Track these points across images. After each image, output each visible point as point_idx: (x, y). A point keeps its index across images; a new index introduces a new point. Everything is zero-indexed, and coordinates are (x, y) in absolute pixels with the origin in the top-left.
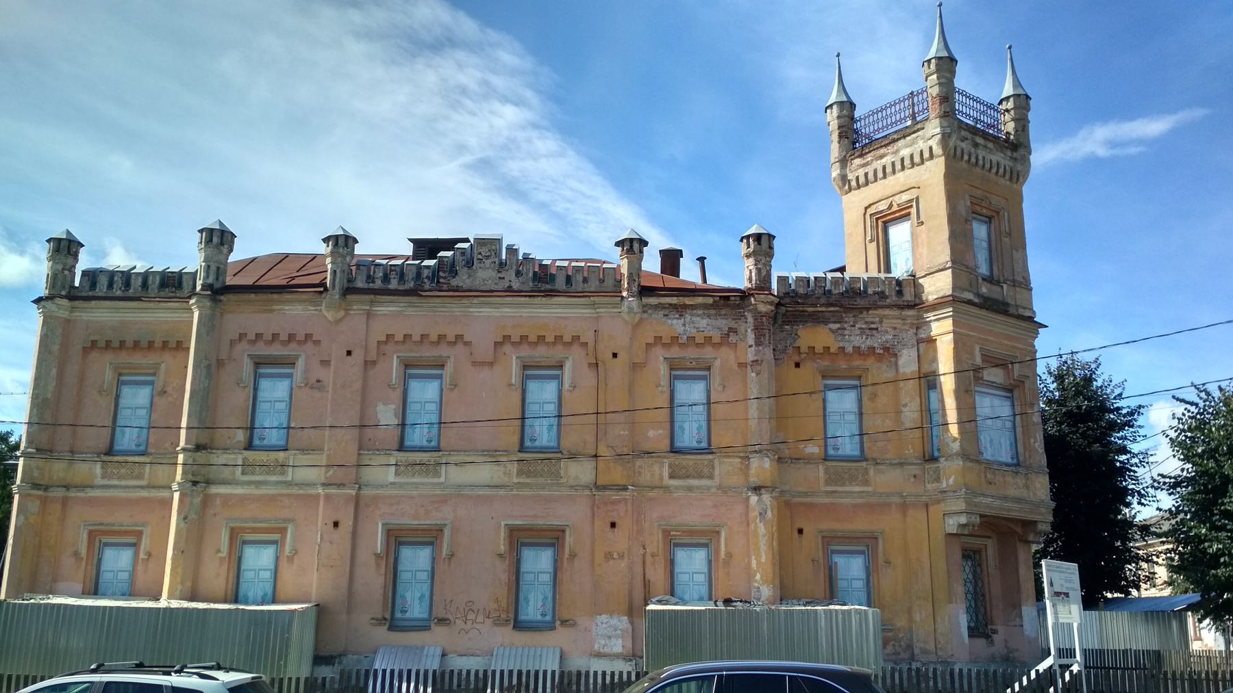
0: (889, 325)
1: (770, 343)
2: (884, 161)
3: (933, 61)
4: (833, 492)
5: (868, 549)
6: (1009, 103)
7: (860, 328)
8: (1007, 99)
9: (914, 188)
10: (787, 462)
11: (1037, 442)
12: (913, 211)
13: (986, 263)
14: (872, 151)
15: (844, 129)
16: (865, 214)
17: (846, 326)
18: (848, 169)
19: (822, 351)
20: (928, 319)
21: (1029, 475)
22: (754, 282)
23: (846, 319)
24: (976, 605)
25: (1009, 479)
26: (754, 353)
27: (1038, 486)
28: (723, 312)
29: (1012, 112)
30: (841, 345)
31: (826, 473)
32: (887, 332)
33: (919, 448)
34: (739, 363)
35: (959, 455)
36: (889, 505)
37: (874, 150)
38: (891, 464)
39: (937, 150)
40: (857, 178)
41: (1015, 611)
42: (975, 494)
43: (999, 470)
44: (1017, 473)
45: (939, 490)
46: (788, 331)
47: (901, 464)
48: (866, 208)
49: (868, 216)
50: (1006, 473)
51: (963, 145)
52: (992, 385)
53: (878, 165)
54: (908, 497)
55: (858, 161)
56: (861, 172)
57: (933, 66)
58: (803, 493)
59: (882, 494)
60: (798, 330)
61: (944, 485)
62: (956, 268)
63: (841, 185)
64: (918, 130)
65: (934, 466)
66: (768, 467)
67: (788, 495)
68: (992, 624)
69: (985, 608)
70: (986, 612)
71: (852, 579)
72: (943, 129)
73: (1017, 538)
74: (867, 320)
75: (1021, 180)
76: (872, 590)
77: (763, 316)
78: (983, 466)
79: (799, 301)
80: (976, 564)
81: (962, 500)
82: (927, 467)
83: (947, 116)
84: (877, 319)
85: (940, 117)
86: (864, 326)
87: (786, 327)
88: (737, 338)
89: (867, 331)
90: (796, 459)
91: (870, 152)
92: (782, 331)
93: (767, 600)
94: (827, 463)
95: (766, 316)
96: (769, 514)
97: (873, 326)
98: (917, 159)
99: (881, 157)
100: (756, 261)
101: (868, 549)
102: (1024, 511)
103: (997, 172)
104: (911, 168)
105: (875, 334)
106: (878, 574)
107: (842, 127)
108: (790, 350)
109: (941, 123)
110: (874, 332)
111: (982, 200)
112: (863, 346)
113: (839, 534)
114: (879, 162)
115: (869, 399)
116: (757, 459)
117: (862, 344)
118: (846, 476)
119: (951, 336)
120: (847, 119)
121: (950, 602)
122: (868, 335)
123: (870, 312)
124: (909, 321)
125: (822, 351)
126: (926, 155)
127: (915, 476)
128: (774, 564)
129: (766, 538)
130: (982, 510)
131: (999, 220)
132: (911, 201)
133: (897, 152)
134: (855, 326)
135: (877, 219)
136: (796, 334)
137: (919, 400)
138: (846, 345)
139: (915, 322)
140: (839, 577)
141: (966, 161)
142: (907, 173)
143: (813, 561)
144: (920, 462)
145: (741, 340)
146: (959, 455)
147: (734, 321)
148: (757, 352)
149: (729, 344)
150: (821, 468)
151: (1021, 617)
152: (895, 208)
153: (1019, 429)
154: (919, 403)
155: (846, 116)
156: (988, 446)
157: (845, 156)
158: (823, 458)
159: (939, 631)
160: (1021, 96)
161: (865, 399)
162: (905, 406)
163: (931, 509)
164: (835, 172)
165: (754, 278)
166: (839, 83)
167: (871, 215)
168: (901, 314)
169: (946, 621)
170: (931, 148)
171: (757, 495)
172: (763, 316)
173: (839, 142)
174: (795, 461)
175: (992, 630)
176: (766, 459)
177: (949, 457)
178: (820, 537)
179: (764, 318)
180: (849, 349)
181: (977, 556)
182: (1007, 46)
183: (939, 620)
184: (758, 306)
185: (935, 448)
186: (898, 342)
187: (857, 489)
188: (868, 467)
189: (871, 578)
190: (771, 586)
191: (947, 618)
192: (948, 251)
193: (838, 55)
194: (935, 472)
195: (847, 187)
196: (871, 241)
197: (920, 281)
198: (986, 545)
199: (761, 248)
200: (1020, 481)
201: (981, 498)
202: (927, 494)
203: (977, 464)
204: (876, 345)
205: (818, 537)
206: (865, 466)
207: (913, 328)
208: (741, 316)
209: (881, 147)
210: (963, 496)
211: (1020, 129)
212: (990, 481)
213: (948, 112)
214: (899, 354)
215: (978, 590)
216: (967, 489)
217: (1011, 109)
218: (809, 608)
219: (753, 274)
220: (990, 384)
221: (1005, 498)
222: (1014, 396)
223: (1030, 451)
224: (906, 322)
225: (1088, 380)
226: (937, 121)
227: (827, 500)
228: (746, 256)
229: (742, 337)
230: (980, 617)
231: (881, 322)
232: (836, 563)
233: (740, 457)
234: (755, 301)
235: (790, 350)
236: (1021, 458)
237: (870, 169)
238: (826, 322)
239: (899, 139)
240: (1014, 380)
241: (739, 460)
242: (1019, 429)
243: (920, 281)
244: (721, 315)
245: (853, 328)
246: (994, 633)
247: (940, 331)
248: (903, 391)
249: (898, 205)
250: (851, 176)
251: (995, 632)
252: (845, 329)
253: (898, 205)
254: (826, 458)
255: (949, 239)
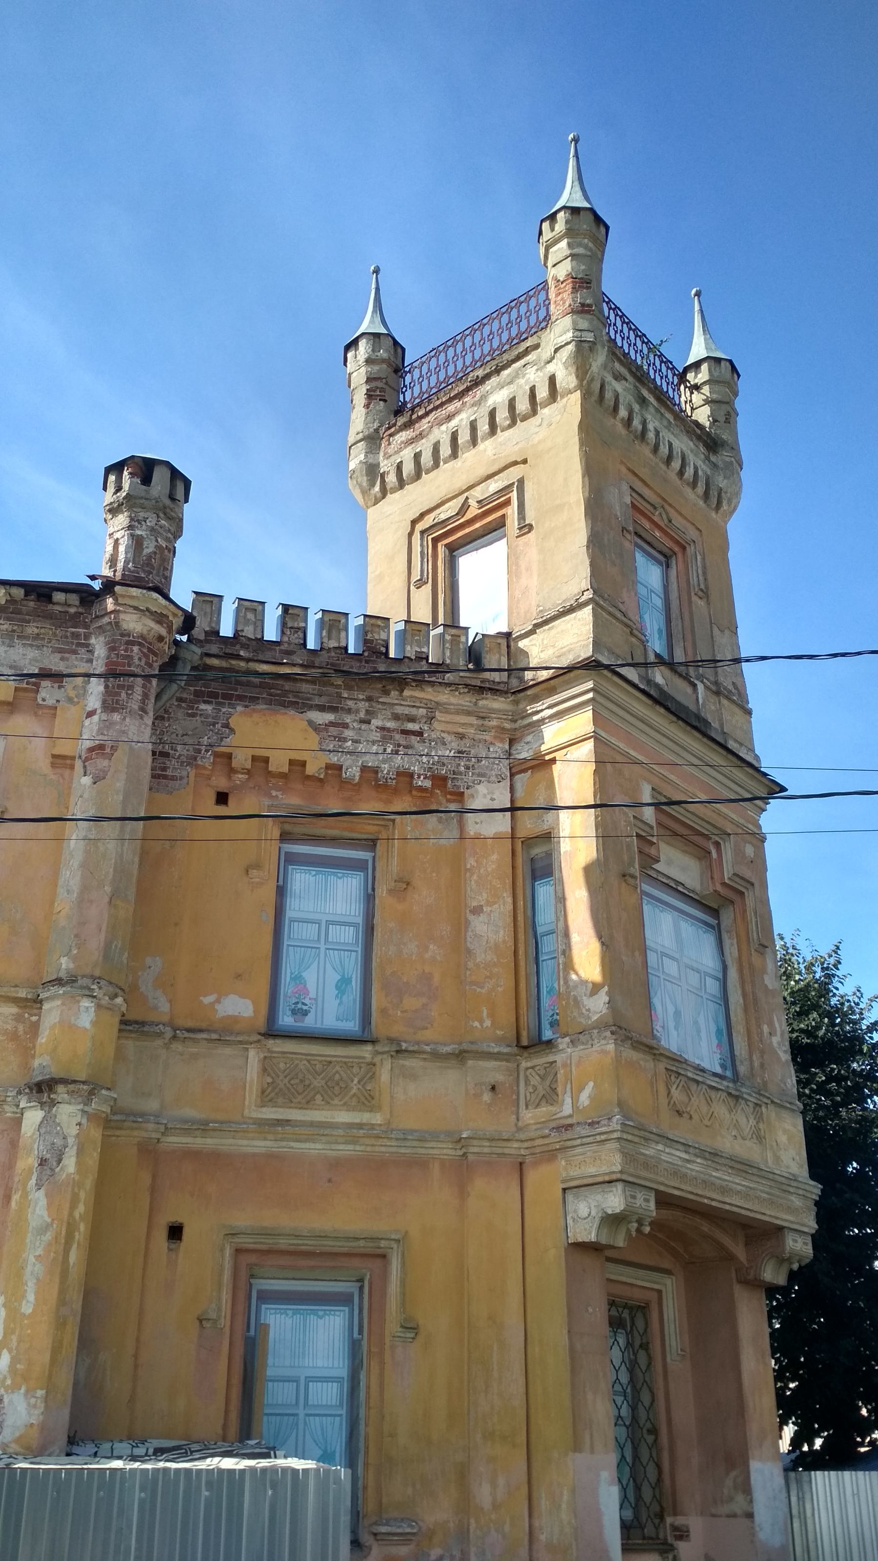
0: (450, 727)
1: (143, 710)
2: (454, 423)
3: (561, 216)
4: (279, 1122)
5: (361, 1288)
6: (700, 376)
7: (383, 729)
8: (697, 365)
9: (515, 463)
10: (160, 1035)
11: (775, 1035)
12: (512, 512)
13: (660, 638)
14: (431, 411)
15: (379, 384)
16: (410, 535)
17: (348, 719)
18: (382, 454)
19: (285, 769)
20: (535, 718)
21: (764, 1109)
22: (120, 565)
23: (350, 703)
24: (636, 1456)
25: (721, 1110)
26: (96, 728)
27: (783, 1139)
28: (31, 629)
29: (706, 390)
30: (334, 759)
31: (265, 1070)
32: (444, 744)
33: (507, 1017)
34: (54, 756)
35: (607, 1026)
36: (421, 1164)
37: (436, 408)
38: (436, 1056)
39: (566, 378)
40: (399, 467)
41: (733, 1474)
42: (647, 1135)
43: (697, 1082)
44: (737, 1098)
45: (553, 1124)
46: (207, 717)
47: (461, 1056)
48: (414, 523)
49: (417, 536)
50: (713, 1094)
51: (618, 387)
52: (674, 888)
53: (442, 434)
54: (475, 1142)
55: (404, 436)
56: (407, 455)
57: (560, 226)
58: (193, 1122)
59: (405, 1132)
60: (231, 714)
61: (567, 1109)
62: (602, 607)
63: (365, 484)
64: (527, 352)
65: (541, 1060)
66: (88, 1025)
67: (151, 1126)
68: (675, 1514)
69: (659, 1467)
70: (659, 1480)
71: (309, 1379)
72: (578, 334)
73: (734, 1275)
74: (399, 710)
75: (725, 506)
76: (362, 1412)
77: (133, 643)
78: (661, 1066)
79: (242, 653)
80: (637, 1343)
81: (614, 1145)
82: (524, 1064)
83: (588, 312)
84: (422, 712)
85: (573, 312)
86: (390, 724)
87: (203, 706)
88: (59, 694)
89: (398, 737)
90: (189, 1030)
91: (427, 414)
92: (193, 715)
93: (17, 1441)
94: (270, 1042)
95: (140, 644)
96: (70, 1163)
97: (411, 726)
98: (523, 406)
99: (450, 417)
100: (132, 519)
101: (361, 1288)
102: (758, 1198)
103: (681, 473)
104: (510, 426)
105: (416, 745)
106: (382, 1363)
107: (375, 379)
108: (207, 760)
109: (574, 323)
110: (414, 739)
111: (655, 508)
112: (385, 767)
113: (283, 1243)
114: (444, 428)
115: (391, 892)
116: (59, 1002)
117: (384, 761)
118: (318, 1082)
119: (589, 745)
120: (384, 366)
121: (577, 1448)
122: (399, 745)
123: (406, 693)
124: (494, 723)
125: (285, 769)
126: (542, 393)
127: (493, 1088)
128: (60, 1323)
129: (48, 1236)
130: (661, 1179)
131: (686, 562)
132: (508, 488)
133: (484, 398)
134: (369, 722)
135: (435, 541)
136: (227, 726)
137: (510, 900)
138: (346, 761)
139: (507, 725)
140: (270, 1372)
141: (623, 419)
142: (499, 440)
143: (201, 1321)
144: (506, 1050)
145: (70, 700)
146: (607, 1026)
147: (59, 655)
148: (107, 725)
149: (37, 709)
150: (254, 1056)
151: (746, 1488)
152: (473, 511)
153: (736, 998)
154: (510, 907)
155: (383, 361)
156: (671, 1024)
157: (377, 431)
158: (263, 1031)
159: (543, 1538)
160: (723, 363)
161: (382, 891)
162: (477, 911)
163: (532, 1176)
164: (357, 459)
165: (122, 556)
166: (374, 311)
167: (422, 532)
168: (476, 704)
169: (564, 1506)
170: (552, 380)
171: (42, 1104)
172: (133, 643)
173: (367, 406)
174: (187, 1035)
175: (675, 1528)
176: (86, 1003)
177: (580, 1035)
178: (228, 1252)
179: (136, 649)
180: (353, 771)
181: (640, 1324)
182: (694, 291)
183: (543, 1504)
184: (122, 616)
185: (545, 1024)
186: (468, 768)
187: (344, 1117)
188: (377, 1060)
189: (363, 1376)
190: (40, 1393)
191: (566, 1497)
192: (585, 570)
193: (377, 271)
194: (543, 1078)
195: (377, 488)
196: (420, 583)
197: (522, 644)
198: (659, 1292)
199: (147, 492)
200: (746, 1121)
201: (660, 1147)
202: (522, 1136)
203: (649, 1058)
204: (416, 769)
205: (222, 1250)
206: (368, 1056)
207: (502, 740)
208: (79, 645)
209: (451, 400)
210: (615, 1135)
211: (722, 419)
212: (679, 1107)
213: (589, 306)
214: (467, 792)
215: (642, 1414)
216: (626, 1117)
217: (704, 383)
218: (161, 1465)
219: (122, 549)
220: (672, 884)
221: (713, 1156)
222: (722, 927)
223: (762, 1052)
224: (486, 723)
225: (824, 989)
226: (568, 321)
227: (260, 1145)
228: (110, 511)
229: (72, 694)
230: (647, 1494)
231: (431, 719)
232: (267, 1326)
233: (16, 1001)
234: (116, 603)
235: (207, 760)
236: (742, 1069)
237: (425, 447)
238: (302, 705)
239: (487, 377)
240: (724, 884)
241: (13, 1010)
242: (736, 998)
243: (522, 644)
244: (26, 638)
245: (364, 726)
246: (680, 1538)
247: (563, 739)
248: (475, 877)
249: (479, 502)
250: (386, 466)
251: (682, 1534)
252: (345, 726)
253: (479, 502)
254: (272, 1032)
255: (588, 547)
